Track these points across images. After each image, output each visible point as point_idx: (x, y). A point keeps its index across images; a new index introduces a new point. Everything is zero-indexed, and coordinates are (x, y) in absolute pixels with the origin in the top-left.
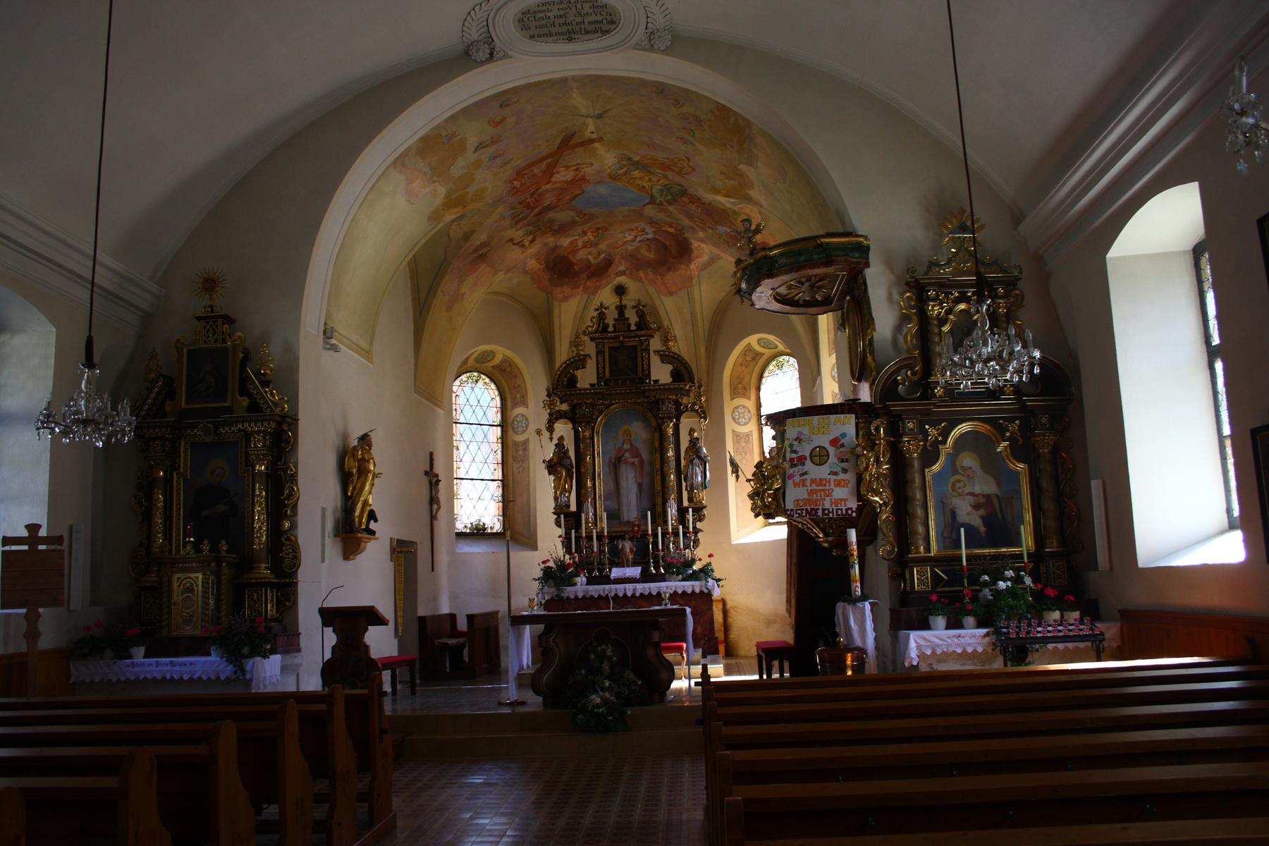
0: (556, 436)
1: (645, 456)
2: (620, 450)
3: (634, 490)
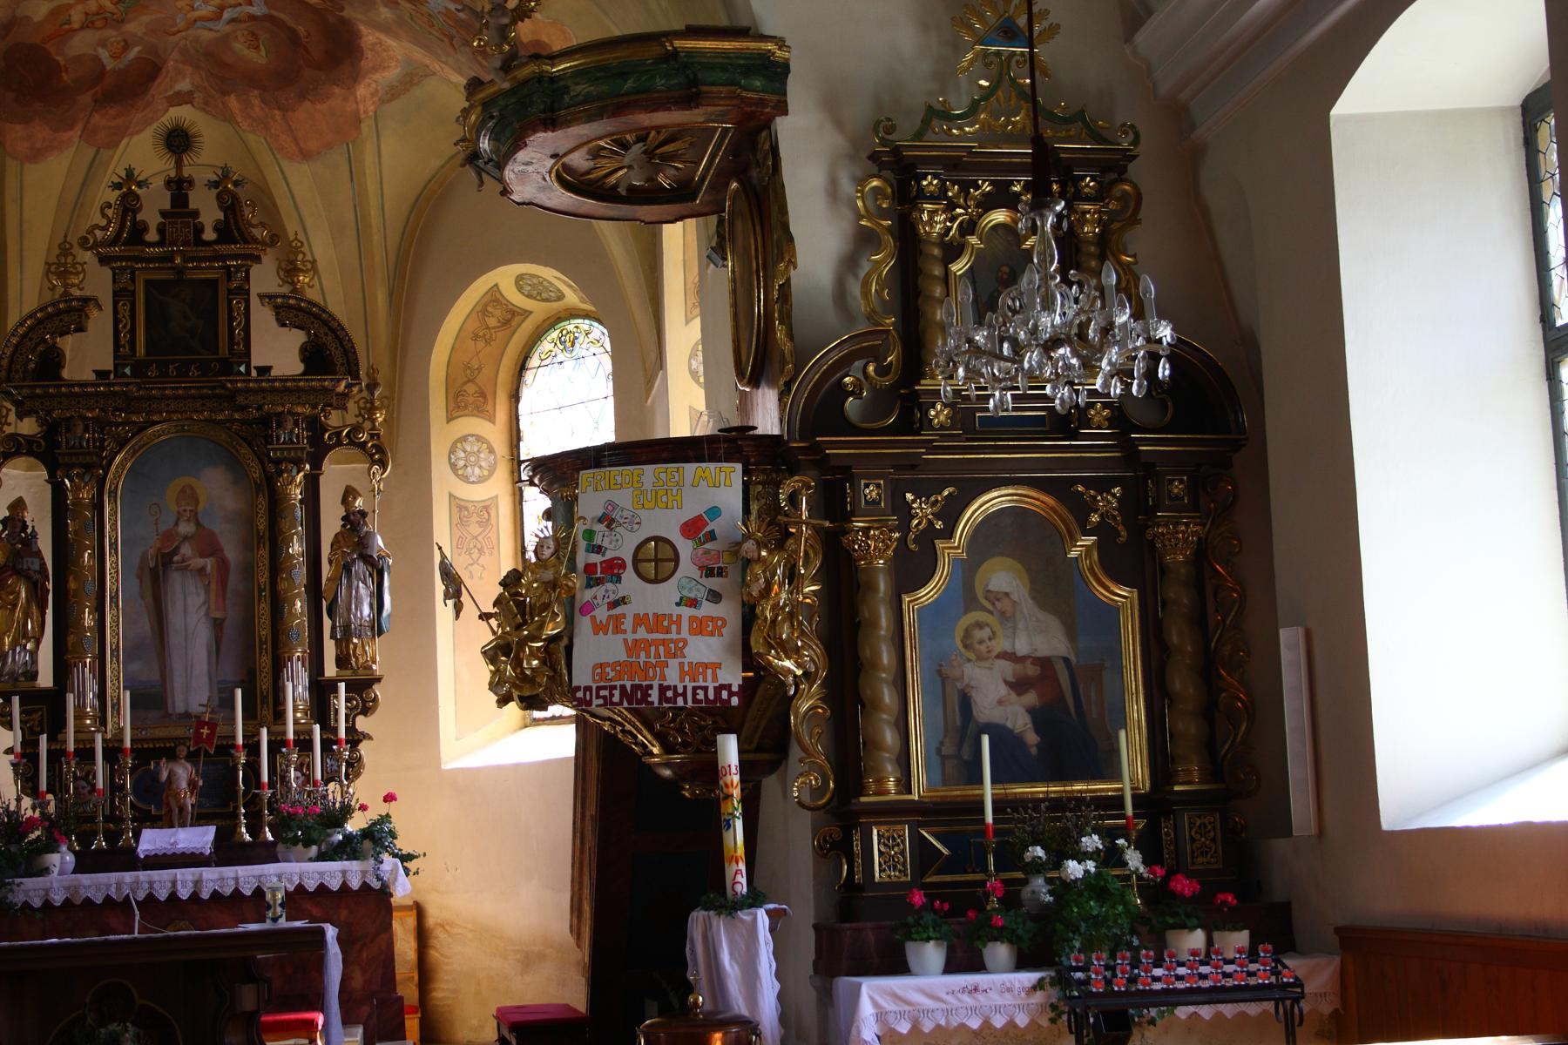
1: (232, 553)
2: (168, 536)
3: (202, 635)
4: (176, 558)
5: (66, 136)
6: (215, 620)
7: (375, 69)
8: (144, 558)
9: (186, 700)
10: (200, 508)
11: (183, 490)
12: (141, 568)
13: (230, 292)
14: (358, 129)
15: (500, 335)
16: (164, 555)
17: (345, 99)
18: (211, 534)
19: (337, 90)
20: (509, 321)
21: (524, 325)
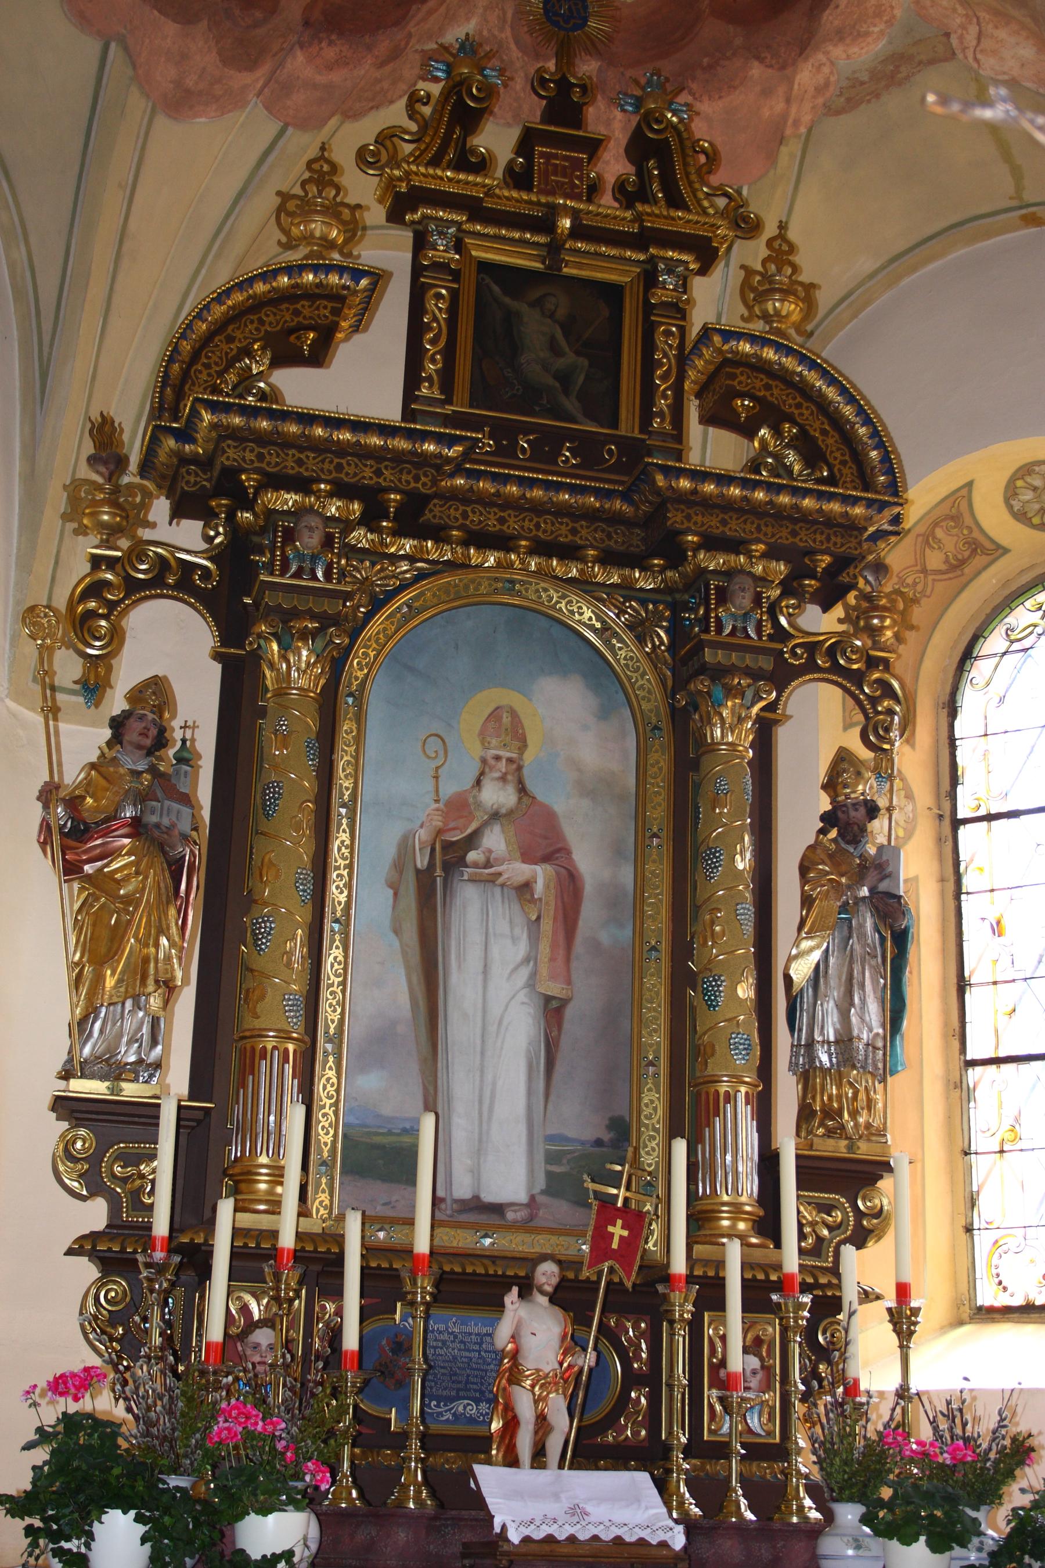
0: (127, 675)
1: (589, 860)
2: (458, 807)
3: (519, 1029)
4: (472, 856)
5: (241, 79)
6: (548, 999)
7: (840, 36)
8: (405, 847)
9: (476, 1172)
10: (529, 757)
11: (495, 715)
12: (399, 865)
13: (648, 308)
14: (772, 158)
15: (940, 587)
16: (448, 846)
17: (767, 92)
18: (550, 818)
19: (756, 70)
20: (962, 562)
21: (985, 575)
